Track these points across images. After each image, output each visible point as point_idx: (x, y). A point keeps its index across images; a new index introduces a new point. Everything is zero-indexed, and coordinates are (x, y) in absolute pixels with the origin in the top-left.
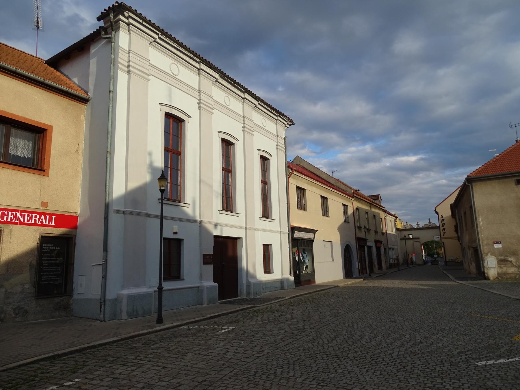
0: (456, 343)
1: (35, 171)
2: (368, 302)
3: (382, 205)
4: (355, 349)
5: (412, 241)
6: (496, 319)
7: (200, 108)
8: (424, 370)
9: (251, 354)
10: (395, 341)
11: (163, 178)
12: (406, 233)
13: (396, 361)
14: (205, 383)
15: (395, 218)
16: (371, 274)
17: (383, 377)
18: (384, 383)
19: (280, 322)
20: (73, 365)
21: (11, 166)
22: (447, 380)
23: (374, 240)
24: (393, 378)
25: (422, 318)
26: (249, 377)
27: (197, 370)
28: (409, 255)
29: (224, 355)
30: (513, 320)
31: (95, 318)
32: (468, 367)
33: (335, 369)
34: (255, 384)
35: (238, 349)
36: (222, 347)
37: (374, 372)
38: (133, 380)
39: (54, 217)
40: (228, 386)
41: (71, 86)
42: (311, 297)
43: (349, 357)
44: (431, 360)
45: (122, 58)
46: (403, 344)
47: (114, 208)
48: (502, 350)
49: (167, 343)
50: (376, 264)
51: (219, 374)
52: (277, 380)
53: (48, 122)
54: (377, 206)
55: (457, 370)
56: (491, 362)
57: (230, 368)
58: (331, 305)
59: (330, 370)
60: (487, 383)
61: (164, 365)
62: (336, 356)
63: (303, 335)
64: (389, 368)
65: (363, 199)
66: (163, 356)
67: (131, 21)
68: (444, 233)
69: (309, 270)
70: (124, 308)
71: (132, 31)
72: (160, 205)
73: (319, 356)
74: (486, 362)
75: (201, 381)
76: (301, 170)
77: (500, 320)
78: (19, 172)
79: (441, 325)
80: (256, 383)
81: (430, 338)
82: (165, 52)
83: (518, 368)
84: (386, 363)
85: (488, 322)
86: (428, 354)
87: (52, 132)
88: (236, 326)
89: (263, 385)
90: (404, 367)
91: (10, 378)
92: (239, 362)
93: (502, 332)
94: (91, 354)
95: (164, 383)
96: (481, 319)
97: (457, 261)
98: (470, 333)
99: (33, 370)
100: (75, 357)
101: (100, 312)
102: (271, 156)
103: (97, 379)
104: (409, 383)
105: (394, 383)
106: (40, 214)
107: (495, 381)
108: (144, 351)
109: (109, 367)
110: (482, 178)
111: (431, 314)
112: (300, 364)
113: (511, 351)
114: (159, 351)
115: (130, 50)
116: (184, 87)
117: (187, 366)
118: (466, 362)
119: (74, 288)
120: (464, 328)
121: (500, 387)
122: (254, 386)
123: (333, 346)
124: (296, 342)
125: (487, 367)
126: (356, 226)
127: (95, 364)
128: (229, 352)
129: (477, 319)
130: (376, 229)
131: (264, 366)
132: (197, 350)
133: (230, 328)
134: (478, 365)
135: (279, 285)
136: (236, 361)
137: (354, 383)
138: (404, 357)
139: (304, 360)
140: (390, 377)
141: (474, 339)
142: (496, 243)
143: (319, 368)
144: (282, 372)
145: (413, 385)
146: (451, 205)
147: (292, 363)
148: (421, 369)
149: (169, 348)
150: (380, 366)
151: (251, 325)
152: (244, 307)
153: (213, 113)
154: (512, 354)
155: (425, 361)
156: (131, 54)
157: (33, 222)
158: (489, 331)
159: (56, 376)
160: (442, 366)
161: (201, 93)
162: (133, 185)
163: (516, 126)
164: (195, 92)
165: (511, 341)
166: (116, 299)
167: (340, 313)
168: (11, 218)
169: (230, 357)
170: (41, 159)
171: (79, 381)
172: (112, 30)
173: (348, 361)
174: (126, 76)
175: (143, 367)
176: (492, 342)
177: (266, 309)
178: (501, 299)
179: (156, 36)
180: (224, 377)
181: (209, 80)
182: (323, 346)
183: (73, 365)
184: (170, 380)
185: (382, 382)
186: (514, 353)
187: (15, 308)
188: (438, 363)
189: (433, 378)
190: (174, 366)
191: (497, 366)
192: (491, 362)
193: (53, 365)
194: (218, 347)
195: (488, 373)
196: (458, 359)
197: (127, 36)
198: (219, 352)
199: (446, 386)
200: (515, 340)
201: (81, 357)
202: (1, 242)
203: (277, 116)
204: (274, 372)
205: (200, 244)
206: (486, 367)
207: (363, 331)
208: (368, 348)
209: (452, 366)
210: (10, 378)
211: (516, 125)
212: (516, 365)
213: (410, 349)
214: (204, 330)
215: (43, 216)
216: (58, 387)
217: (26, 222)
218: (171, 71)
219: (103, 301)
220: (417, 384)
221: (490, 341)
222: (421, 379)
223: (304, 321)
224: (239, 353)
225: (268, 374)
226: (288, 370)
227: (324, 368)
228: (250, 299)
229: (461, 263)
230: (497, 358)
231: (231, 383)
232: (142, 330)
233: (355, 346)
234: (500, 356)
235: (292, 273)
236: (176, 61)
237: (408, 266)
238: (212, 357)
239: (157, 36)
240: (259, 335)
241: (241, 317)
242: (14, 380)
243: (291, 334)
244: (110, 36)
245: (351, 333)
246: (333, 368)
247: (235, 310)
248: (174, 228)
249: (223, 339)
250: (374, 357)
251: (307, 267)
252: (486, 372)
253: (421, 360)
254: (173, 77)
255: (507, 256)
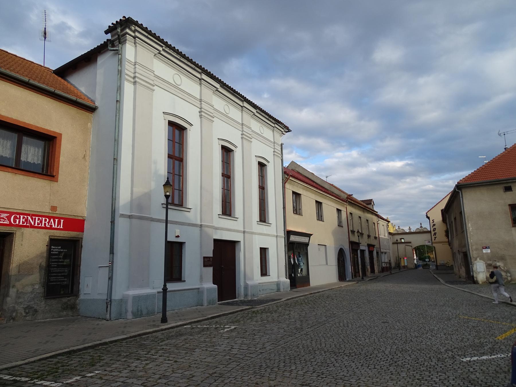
0: (443, 342)
1: (45, 177)
2: (361, 304)
3: (375, 209)
4: (350, 347)
5: (404, 245)
6: (482, 320)
7: (201, 116)
8: (413, 364)
9: (255, 350)
10: (387, 340)
11: (167, 184)
12: (398, 237)
13: (388, 357)
14: (215, 375)
15: (387, 222)
16: (364, 277)
17: (377, 371)
18: (377, 375)
19: (278, 322)
20: (90, 359)
21: (23, 173)
22: (434, 373)
23: (367, 244)
24: (386, 371)
25: (413, 319)
26: (255, 370)
27: (206, 363)
28: (401, 258)
29: (229, 351)
30: (498, 322)
31: (101, 317)
32: (454, 362)
33: (333, 363)
34: (261, 376)
35: (242, 346)
36: (226, 344)
37: (368, 366)
38: (149, 372)
39: (62, 221)
40: (237, 377)
41: (79, 95)
42: (306, 299)
43: (345, 353)
44: (421, 356)
45: (128, 69)
46: (395, 342)
47: (121, 212)
48: (485, 348)
49: (174, 341)
50: (369, 267)
51: (227, 368)
52: (280, 373)
53: (57, 131)
54: (370, 210)
55: (443, 365)
56: (475, 358)
57: (236, 362)
58: (327, 307)
59: (329, 364)
60: (470, 376)
61: (175, 359)
62: (333, 353)
63: (301, 334)
64: (382, 363)
65: (356, 204)
66: (173, 352)
67: (137, 34)
68: (435, 238)
69: (304, 273)
70: (130, 309)
71: (138, 43)
72: (165, 210)
73: (317, 352)
74: (470, 358)
75: (211, 373)
76: (297, 175)
77: (486, 321)
78: (30, 178)
79: (430, 326)
80: (262, 375)
81: (420, 337)
82: (169, 63)
83: (499, 363)
84: (380, 359)
85: (475, 323)
86: (418, 351)
87: (61, 139)
88: (237, 326)
89: (268, 377)
90: (396, 362)
91: (34, 370)
92: (244, 357)
93: (487, 333)
94: (103, 350)
95: (177, 375)
96: (469, 320)
97: (447, 265)
98: (457, 333)
99: (53, 364)
100: (90, 353)
101: (107, 311)
102: (268, 162)
103: (116, 371)
104: (400, 376)
105: (387, 375)
106: (50, 218)
107: (477, 374)
108: (154, 347)
109: (125, 361)
110: (472, 185)
111: (421, 315)
112: (300, 359)
113: (494, 349)
114: (168, 348)
115: (136, 62)
116: (186, 96)
117: (196, 360)
118: (452, 358)
119: (80, 288)
120: (452, 328)
121: (482, 379)
122: (260, 377)
123: (330, 344)
124: (296, 340)
125: (471, 362)
126: (350, 230)
127: (111, 358)
128: (233, 348)
129: (464, 321)
130: (369, 233)
131: (268, 361)
132: (204, 347)
133: (232, 327)
134: (462, 361)
135: (275, 287)
136: (241, 357)
137: (350, 375)
138: (395, 354)
139: (303, 356)
140: (383, 371)
141: (461, 339)
142: (485, 248)
143: (318, 362)
144: (284, 366)
145: (404, 377)
146: (442, 210)
147: (293, 358)
148: (411, 364)
149: (177, 344)
150: (374, 361)
151: (251, 324)
152: (243, 308)
153: (213, 121)
154: (495, 351)
155: (415, 357)
156: (137, 66)
157: (43, 226)
158: (475, 332)
159: (77, 368)
160: (430, 361)
161: (202, 102)
162: (139, 190)
163: (504, 134)
164: (132, 43)
165: (495, 341)
166: (121, 299)
167: (335, 314)
168: (23, 221)
169: (235, 353)
170: (51, 166)
171: (99, 373)
172: (119, 43)
173: (344, 357)
174: (132, 86)
175: (156, 361)
176: (477, 341)
177: (264, 310)
178: (488, 302)
179: (161, 49)
180: (232, 370)
181: (210, 90)
182: (321, 344)
183: (90, 359)
184: (183, 372)
185: (376, 375)
186: (496, 350)
187: (26, 307)
188: (426, 359)
189: (421, 372)
190: (184, 361)
191: (480, 362)
192: (475, 358)
193: (70, 359)
194: (223, 344)
195: (472, 367)
196: (445, 356)
197: (133, 49)
198: (225, 349)
199: (433, 378)
200: (499, 339)
201: (95, 352)
202: (14, 244)
203: (274, 123)
204: (277, 366)
205: (201, 247)
206: (470, 363)
207: (358, 331)
208: (362, 345)
209: (439, 362)
210: (34, 370)
211: (505, 133)
212: (498, 361)
213: (401, 347)
214: (208, 329)
215: (52, 220)
216: (81, 378)
217: (36, 225)
218: (174, 81)
219: (109, 302)
220: (407, 377)
221: (476, 340)
222: (410, 372)
223: (302, 321)
224: (243, 349)
225: (271, 367)
226: (290, 364)
227: (323, 363)
228: (247, 300)
229: (451, 268)
230: (481, 355)
231: (239, 375)
232: (148, 329)
233: (350, 344)
234: (484, 353)
235: (288, 275)
236: (179, 72)
237: (400, 270)
238: (218, 352)
239: (162, 49)
240: (260, 334)
241: (241, 318)
242: (39, 372)
243: (291, 333)
244: (117, 48)
245: (346, 332)
246: (331, 363)
247: (234, 311)
248: (176, 232)
249: (227, 337)
250: (368, 353)
251: (302, 270)
252: (470, 367)
253: (411, 356)
254: (176, 87)
255: (495, 261)
